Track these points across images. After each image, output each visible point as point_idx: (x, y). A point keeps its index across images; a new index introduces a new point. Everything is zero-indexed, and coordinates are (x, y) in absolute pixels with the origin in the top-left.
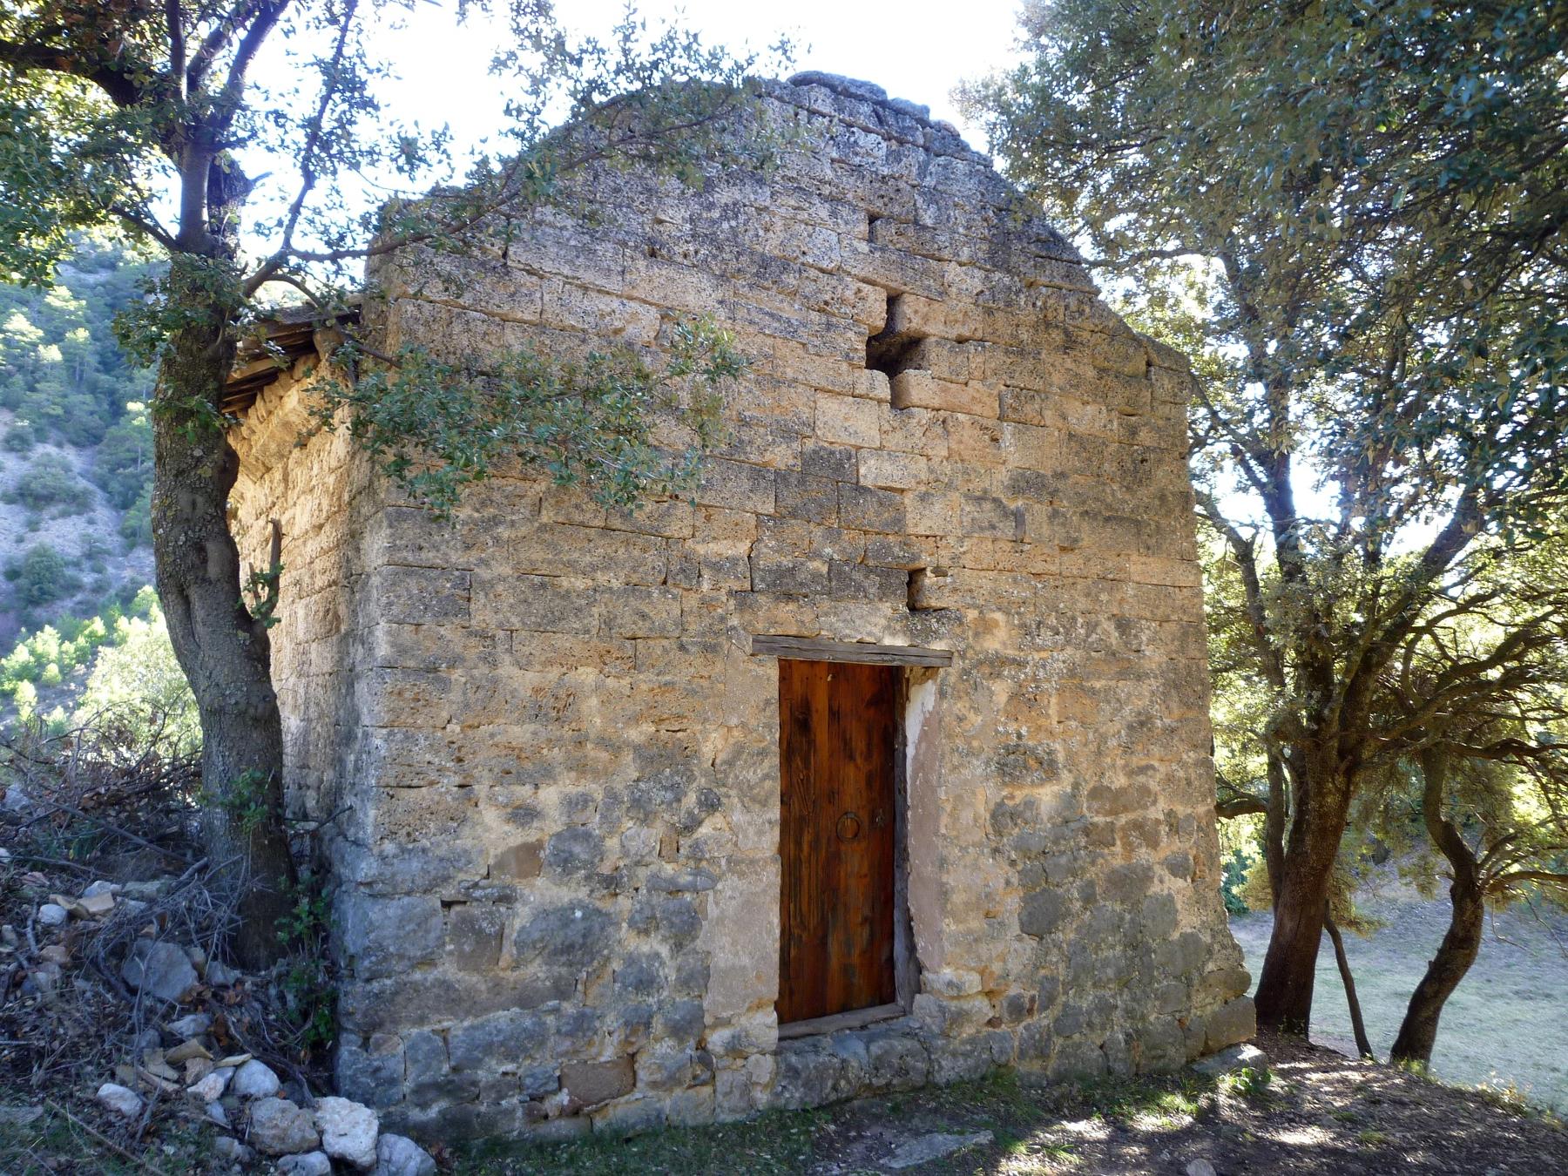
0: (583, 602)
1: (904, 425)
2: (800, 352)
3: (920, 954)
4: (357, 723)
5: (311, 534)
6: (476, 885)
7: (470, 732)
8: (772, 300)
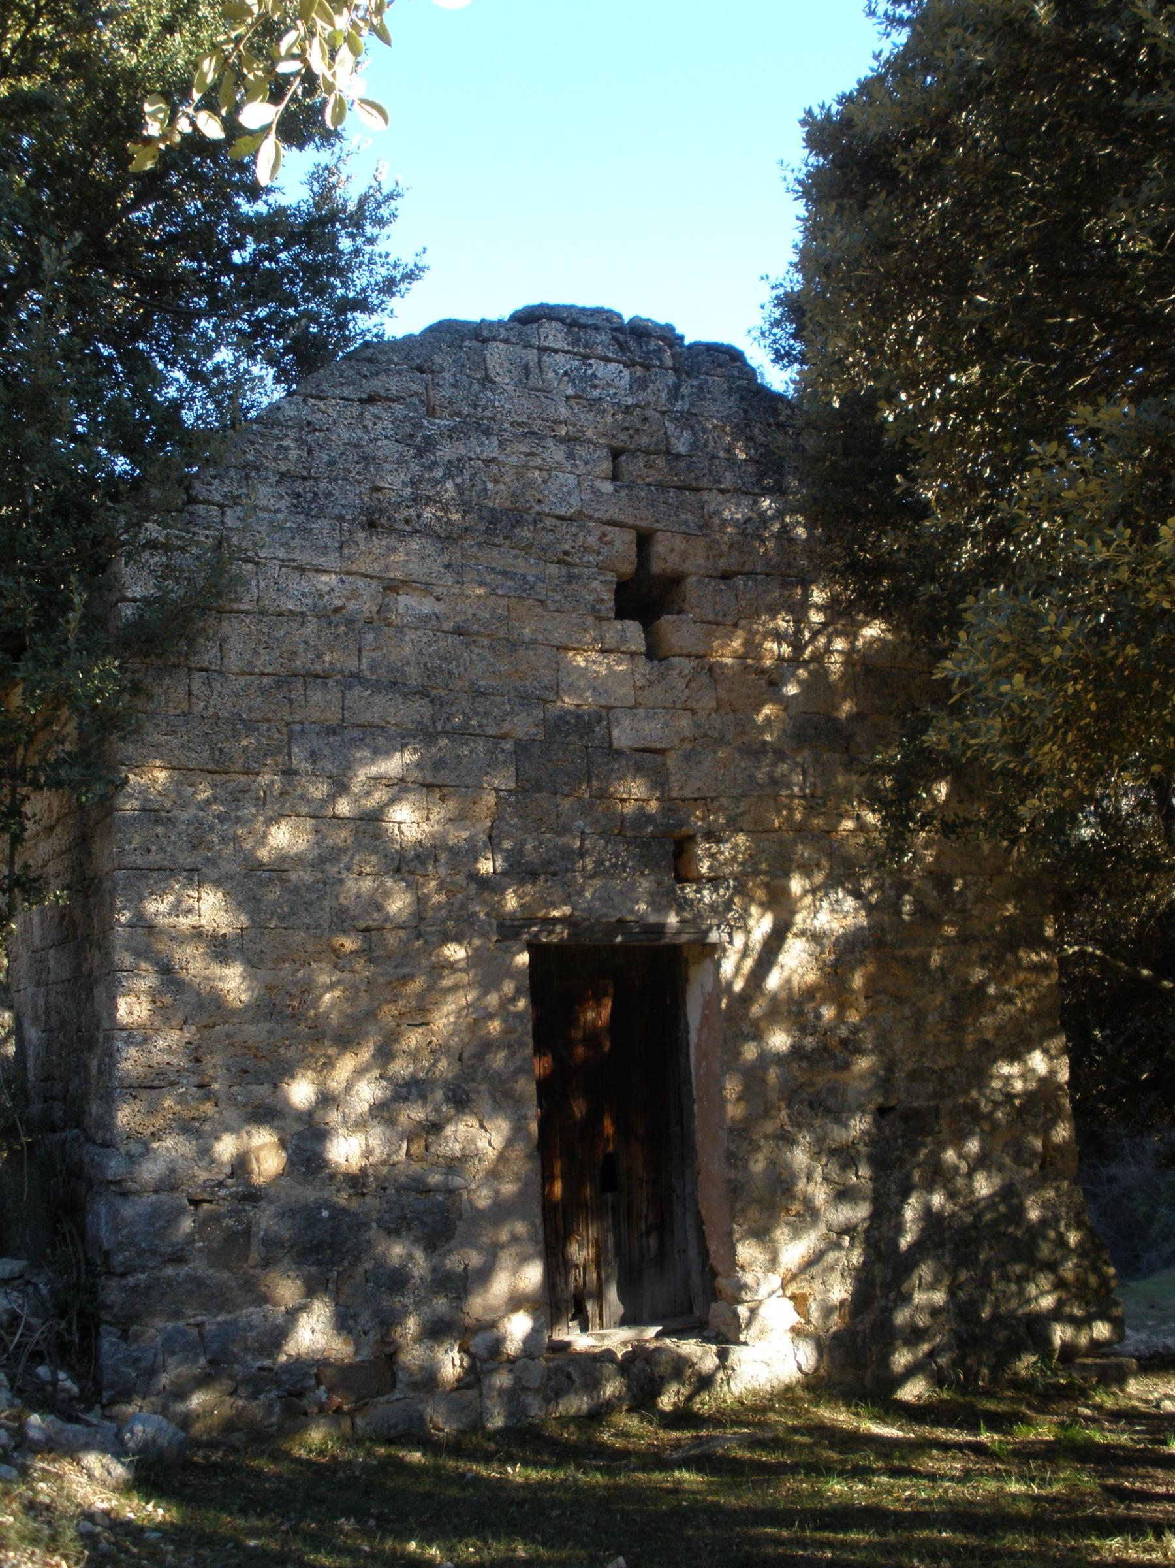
0: (314, 896)
1: (663, 676)
2: (539, 610)
3: (713, 1260)
4: (97, 1028)
5: (42, 835)
6: (221, 1184)
7: (206, 1032)
8: (502, 558)
